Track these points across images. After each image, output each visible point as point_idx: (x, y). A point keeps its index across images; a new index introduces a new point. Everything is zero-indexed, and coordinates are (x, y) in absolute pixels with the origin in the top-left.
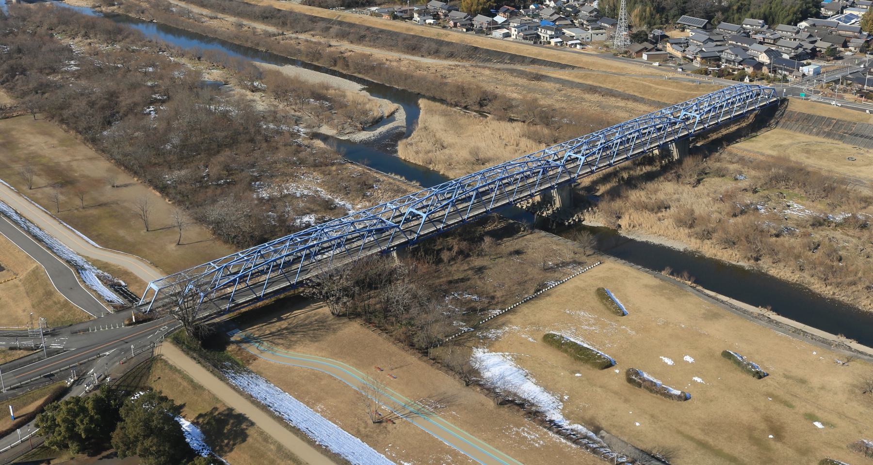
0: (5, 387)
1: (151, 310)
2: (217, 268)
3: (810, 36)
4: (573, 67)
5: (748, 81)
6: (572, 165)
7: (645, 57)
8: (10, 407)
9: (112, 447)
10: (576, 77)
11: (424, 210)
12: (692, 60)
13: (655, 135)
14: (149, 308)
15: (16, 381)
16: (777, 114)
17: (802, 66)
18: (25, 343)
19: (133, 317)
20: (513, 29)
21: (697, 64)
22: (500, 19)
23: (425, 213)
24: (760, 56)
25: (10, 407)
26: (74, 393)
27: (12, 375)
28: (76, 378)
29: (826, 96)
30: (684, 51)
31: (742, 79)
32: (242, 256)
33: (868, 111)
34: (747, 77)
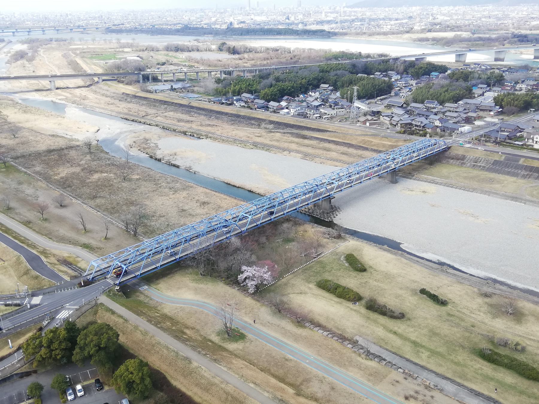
0: (5, 329)
1: (93, 278)
2: (132, 251)
3: (465, 109)
4: (327, 131)
5: (429, 137)
6: (330, 187)
7: (368, 124)
8: (9, 340)
9: (401, 124)
10: (329, 136)
11: (249, 214)
12: (395, 126)
13: (376, 169)
14: (91, 276)
15: (12, 325)
16: (180, 28)
17: (460, 127)
18: (15, 302)
19: (82, 282)
20: (291, 110)
21: (398, 128)
22: (283, 104)
23: (250, 215)
24: (435, 122)
25: (9, 340)
26: (494, 70)
27: (8, 321)
28: (49, 321)
29: (475, 144)
30: (391, 120)
31: (425, 136)
32: (129, 249)
33: (500, 153)
34: (428, 135)
